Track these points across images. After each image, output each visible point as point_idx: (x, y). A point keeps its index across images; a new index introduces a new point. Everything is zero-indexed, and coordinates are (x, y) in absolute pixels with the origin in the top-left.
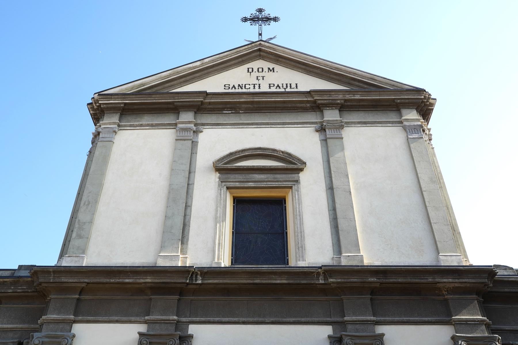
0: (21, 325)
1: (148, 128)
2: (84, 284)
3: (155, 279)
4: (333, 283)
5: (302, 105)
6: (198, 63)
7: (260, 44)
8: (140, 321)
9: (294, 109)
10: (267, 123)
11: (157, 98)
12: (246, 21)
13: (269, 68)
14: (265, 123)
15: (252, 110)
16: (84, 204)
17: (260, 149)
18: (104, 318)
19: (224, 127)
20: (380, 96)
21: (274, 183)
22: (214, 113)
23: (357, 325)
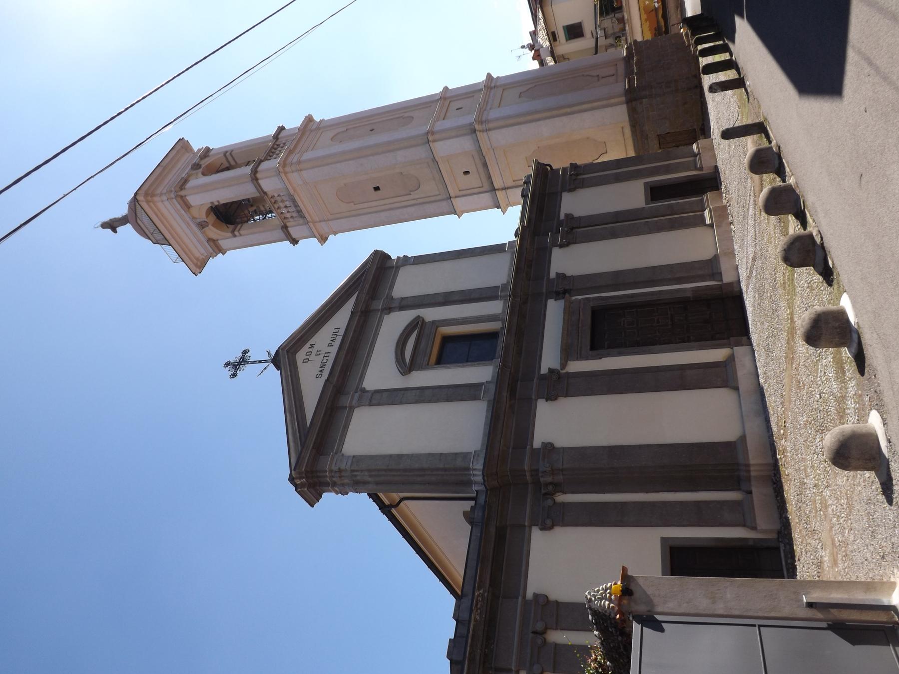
13: (309, 348)
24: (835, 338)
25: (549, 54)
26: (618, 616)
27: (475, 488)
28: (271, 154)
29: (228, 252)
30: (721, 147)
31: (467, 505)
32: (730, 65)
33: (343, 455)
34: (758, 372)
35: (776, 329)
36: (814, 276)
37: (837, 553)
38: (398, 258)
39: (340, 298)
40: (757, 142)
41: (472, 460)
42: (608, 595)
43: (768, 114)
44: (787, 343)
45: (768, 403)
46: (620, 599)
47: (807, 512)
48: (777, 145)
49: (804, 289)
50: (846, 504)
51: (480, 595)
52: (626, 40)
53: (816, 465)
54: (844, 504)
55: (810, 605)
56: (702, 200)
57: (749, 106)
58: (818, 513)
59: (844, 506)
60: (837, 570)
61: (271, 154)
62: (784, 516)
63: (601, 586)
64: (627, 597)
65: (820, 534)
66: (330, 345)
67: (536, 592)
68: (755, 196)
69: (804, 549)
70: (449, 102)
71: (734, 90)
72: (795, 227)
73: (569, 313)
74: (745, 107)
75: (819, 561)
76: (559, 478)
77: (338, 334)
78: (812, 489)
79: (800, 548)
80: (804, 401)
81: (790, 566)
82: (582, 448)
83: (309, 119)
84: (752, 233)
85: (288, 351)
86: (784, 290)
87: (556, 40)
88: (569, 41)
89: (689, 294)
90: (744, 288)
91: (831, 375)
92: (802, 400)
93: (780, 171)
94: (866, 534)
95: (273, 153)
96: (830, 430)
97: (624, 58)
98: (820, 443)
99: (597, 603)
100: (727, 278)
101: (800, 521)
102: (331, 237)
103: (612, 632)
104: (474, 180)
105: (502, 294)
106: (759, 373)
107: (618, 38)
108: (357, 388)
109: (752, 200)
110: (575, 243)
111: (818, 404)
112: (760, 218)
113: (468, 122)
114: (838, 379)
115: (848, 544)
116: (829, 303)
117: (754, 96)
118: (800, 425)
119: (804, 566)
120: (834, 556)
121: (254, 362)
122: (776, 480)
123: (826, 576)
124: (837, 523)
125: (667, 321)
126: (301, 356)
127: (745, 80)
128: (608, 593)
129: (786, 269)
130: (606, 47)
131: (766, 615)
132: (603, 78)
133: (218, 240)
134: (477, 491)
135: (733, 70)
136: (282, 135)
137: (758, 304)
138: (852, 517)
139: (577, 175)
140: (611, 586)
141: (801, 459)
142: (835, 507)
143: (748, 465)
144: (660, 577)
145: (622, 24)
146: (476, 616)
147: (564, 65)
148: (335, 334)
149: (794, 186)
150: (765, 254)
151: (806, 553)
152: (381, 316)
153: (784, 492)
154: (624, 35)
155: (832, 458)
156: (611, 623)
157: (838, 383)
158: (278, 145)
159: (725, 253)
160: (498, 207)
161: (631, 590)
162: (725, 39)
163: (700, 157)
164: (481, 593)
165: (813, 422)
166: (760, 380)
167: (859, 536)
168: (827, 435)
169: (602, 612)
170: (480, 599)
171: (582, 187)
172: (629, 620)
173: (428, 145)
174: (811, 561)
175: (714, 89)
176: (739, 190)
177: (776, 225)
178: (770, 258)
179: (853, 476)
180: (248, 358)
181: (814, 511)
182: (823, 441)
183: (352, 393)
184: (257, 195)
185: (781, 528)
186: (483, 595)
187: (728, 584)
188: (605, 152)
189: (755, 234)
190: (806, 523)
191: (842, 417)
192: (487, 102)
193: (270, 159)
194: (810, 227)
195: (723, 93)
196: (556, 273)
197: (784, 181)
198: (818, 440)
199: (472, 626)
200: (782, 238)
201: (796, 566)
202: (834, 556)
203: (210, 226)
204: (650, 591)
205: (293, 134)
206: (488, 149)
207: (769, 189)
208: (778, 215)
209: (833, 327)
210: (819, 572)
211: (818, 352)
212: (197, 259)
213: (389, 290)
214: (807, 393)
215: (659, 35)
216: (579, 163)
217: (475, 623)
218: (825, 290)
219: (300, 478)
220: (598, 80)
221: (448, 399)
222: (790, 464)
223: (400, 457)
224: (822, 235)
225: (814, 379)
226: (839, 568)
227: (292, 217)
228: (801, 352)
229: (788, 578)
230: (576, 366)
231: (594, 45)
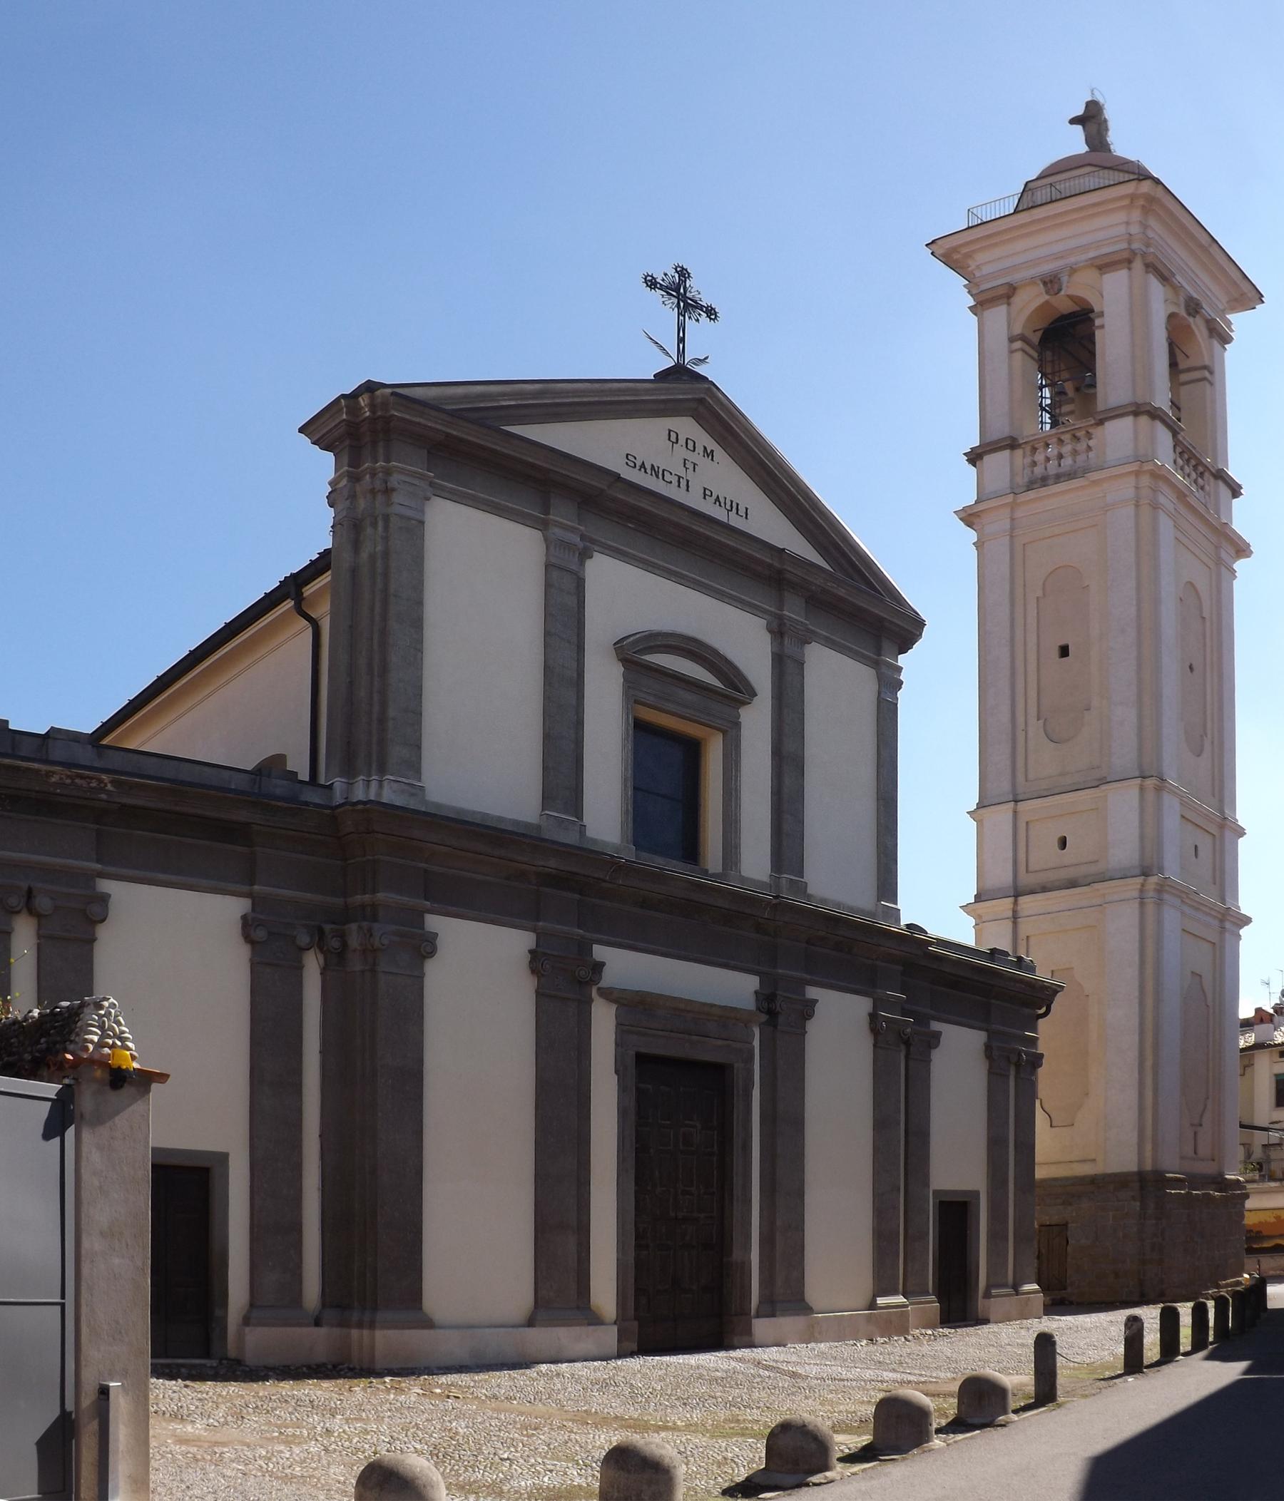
12: (651, 288)
13: (705, 448)
24: (619, 1492)
25: (1261, 1040)
26: (69, 1057)
27: (339, 783)
28: (1186, 456)
30: (1023, 1332)
31: (299, 764)
32: (1170, 1350)
33: (428, 499)
34: (562, 1362)
35: (646, 1400)
36: (747, 1468)
37: (200, 1447)
38: (900, 669)
39: (819, 526)
40: (1020, 1390)
41: (404, 780)
42: (110, 1041)
43: (1069, 1409)
44: (617, 1417)
45: (498, 1373)
46: (103, 1063)
47: (278, 1412)
48: (1008, 1423)
49: (721, 1452)
50: (291, 1474)
51: (102, 785)
52: (1253, 1181)
53: (369, 1437)
54: (293, 1470)
55: (104, 1392)
56: (926, 1293)
57: (1088, 1379)
58: (276, 1429)
59: (289, 1471)
60: (169, 1441)
62: (271, 1373)
63: (128, 1031)
64: (107, 1077)
65: (235, 1426)
67: (111, 900)
68: (918, 1383)
69: (207, 1397)
70: (1214, 833)
71: (1123, 1357)
72: (846, 1444)
73: (727, 1017)
74: (1090, 1373)
75: (185, 1417)
78: (322, 1425)
79: (208, 1392)
80: (498, 1433)
81: (174, 1371)
82: (421, 1017)
83: (1242, 550)
84: (844, 1373)
86: (725, 1419)
88: (1273, 1080)
89: (737, 1255)
90: (738, 1353)
91: (546, 1479)
92: (500, 1430)
93: (958, 1425)
94: (236, 1494)
96: (436, 1467)
97: (1221, 1175)
98: (412, 1449)
99: (94, 1020)
100: (760, 1327)
101: (261, 1398)
102: (972, 535)
103: (38, 1042)
104: (1044, 855)
105: (784, 881)
106: (560, 1365)
107: (1260, 1166)
108: (593, 541)
109: (911, 1378)
110: (875, 1046)
111: (489, 1453)
112: (874, 1389)
113: (1167, 864)
114: (538, 1490)
115: (216, 1465)
116: (689, 1489)
117: (1106, 1388)
118: (450, 1421)
119: (175, 1392)
120: (193, 1441)
121: (681, 327)
122: (341, 1370)
123: (158, 1423)
124: (257, 1455)
125: (685, 1210)
126: (687, 427)
127: (1137, 1376)
128: (114, 1043)
129: (766, 1426)
130: (1249, 1144)
131: (83, 1318)
134: (330, 787)
135: (1159, 1357)
136: (1223, 488)
137: (701, 1376)
138: (267, 1478)
139: (1018, 1066)
140: (129, 1049)
141: (382, 1415)
142: (288, 1456)
143: (372, 1326)
144: (148, 1143)
145: (1281, 1176)
146: (58, 775)
147: (1232, 1063)
148: (733, 507)
149: (926, 1447)
150: (801, 1392)
151: (200, 1399)
152: (765, 611)
153: (317, 1379)
154: (1262, 1179)
155: (383, 1465)
156: (55, 1043)
157: (529, 1489)
158: (1202, 475)
159: (813, 1327)
160: (978, 898)
161: (122, 1087)
162: (1214, 1346)
163: (1012, 1295)
164: (106, 785)
165: (454, 1442)
166: (544, 1365)
167: (232, 1484)
168: (427, 1463)
169: (76, 1028)
170: (94, 784)
171: (991, 1072)
172: (64, 1077)
173: (1137, 774)
174: (185, 1405)
175: (1132, 1325)
176: (934, 1357)
177: (856, 1415)
178: (793, 1401)
179: (346, 1492)
181: (279, 1422)
182: (416, 1455)
184: (1101, 406)
185: (247, 1366)
186: (103, 790)
187: (139, 1264)
188: (1054, 1124)
189: (843, 1380)
190: (257, 1407)
191: (461, 1488)
192: (1197, 909)
193: (1175, 451)
194: (841, 1468)
195: (1122, 1338)
196: (817, 1001)
197: (938, 1431)
198: (418, 1446)
199: (36, 766)
200: (829, 1423)
201: (176, 1380)
202: (193, 1441)
203: (1047, 297)
204: (121, 1121)
206: (1104, 895)
207: (929, 1406)
208: (874, 1418)
209: (642, 1491)
210: (164, 1413)
211: (594, 1465)
212: (969, 255)
213: (827, 637)
214: (513, 1439)
215: (1247, 1238)
216: (1040, 1071)
217: (43, 773)
218: (717, 1484)
219: (373, 406)
220: (1192, 1125)
221: (549, 739)
222: (373, 1397)
223: (417, 624)
224: (825, 1486)
225: (541, 1453)
226: (172, 1445)
228: (597, 1437)
229: (151, 1364)
230: (603, 1021)
231: (1257, 1123)
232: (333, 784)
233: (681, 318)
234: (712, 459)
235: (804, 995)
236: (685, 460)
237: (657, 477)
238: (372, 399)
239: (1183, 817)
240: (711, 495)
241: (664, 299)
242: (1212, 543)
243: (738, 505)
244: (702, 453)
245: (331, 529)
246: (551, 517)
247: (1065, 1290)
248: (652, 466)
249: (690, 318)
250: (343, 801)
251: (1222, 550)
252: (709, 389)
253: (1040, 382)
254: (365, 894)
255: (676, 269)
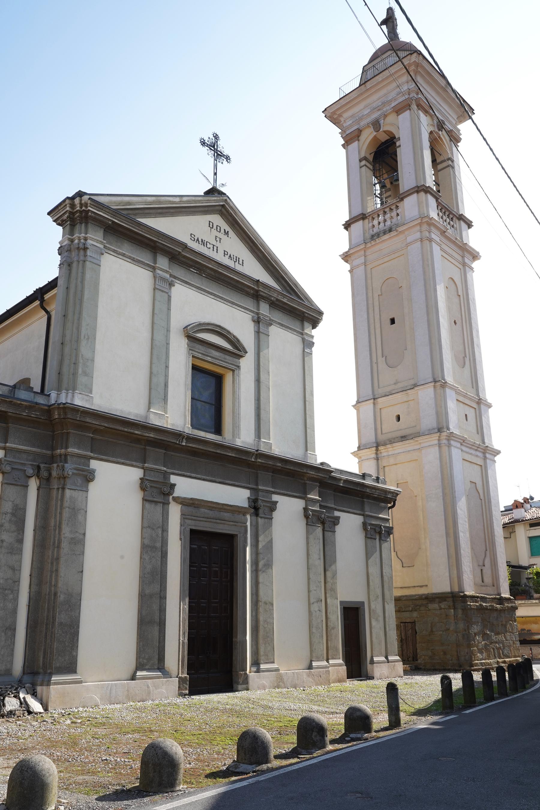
0: (34, 449)
1: (129, 260)
2: (103, 427)
3: (156, 435)
4: (259, 462)
5: (248, 290)
6: (177, 199)
7: (226, 200)
8: (139, 467)
9: (241, 291)
10: (222, 297)
11: (143, 231)
12: (203, 146)
14: (220, 297)
15: (212, 277)
16: (85, 337)
17: (219, 326)
18: (114, 459)
19: (190, 287)
20: (298, 306)
21: (224, 363)
22: (183, 267)
23: (264, 493)
28: (443, 211)
29: (344, 150)
33: (103, 254)
61: (443, 211)
66: (225, 253)
76: (55, 484)
77: (237, 263)
83: (475, 256)
85: (223, 206)
87: (530, 527)
89: (239, 637)
95: (445, 213)
102: (347, 267)
108: (175, 277)
121: (215, 166)
126: (217, 220)
132: (481, 570)
133: (359, 140)
136: (463, 224)
148: (237, 260)
158: (452, 219)
180: (221, 161)
183: (170, 271)
184: (402, 191)
188: (404, 566)
193: (438, 209)
196: (278, 502)
203: (375, 133)
205: (462, 238)
212: (340, 115)
219: (81, 205)
227: (374, 226)
232: (50, 394)
233: (215, 162)
234: (228, 236)
235: (272, 499)
236: (216, 236)
237: (204, 246)
238: (81, 200)
239: (457, 400)
240: (227, 255)
241: (208, 152)
242: (460, 255)
243: (239, 258)
244: (223, 233)
245: (58, 266)
246: (157, 265)
247: (416, 661)
248: (202, 240)
249: (219, 162)
250: (55, 402)
251: (465, 258)
252: (226, 200)
253: (374, 182)
254: (62, 449)
255: (213, 135)
